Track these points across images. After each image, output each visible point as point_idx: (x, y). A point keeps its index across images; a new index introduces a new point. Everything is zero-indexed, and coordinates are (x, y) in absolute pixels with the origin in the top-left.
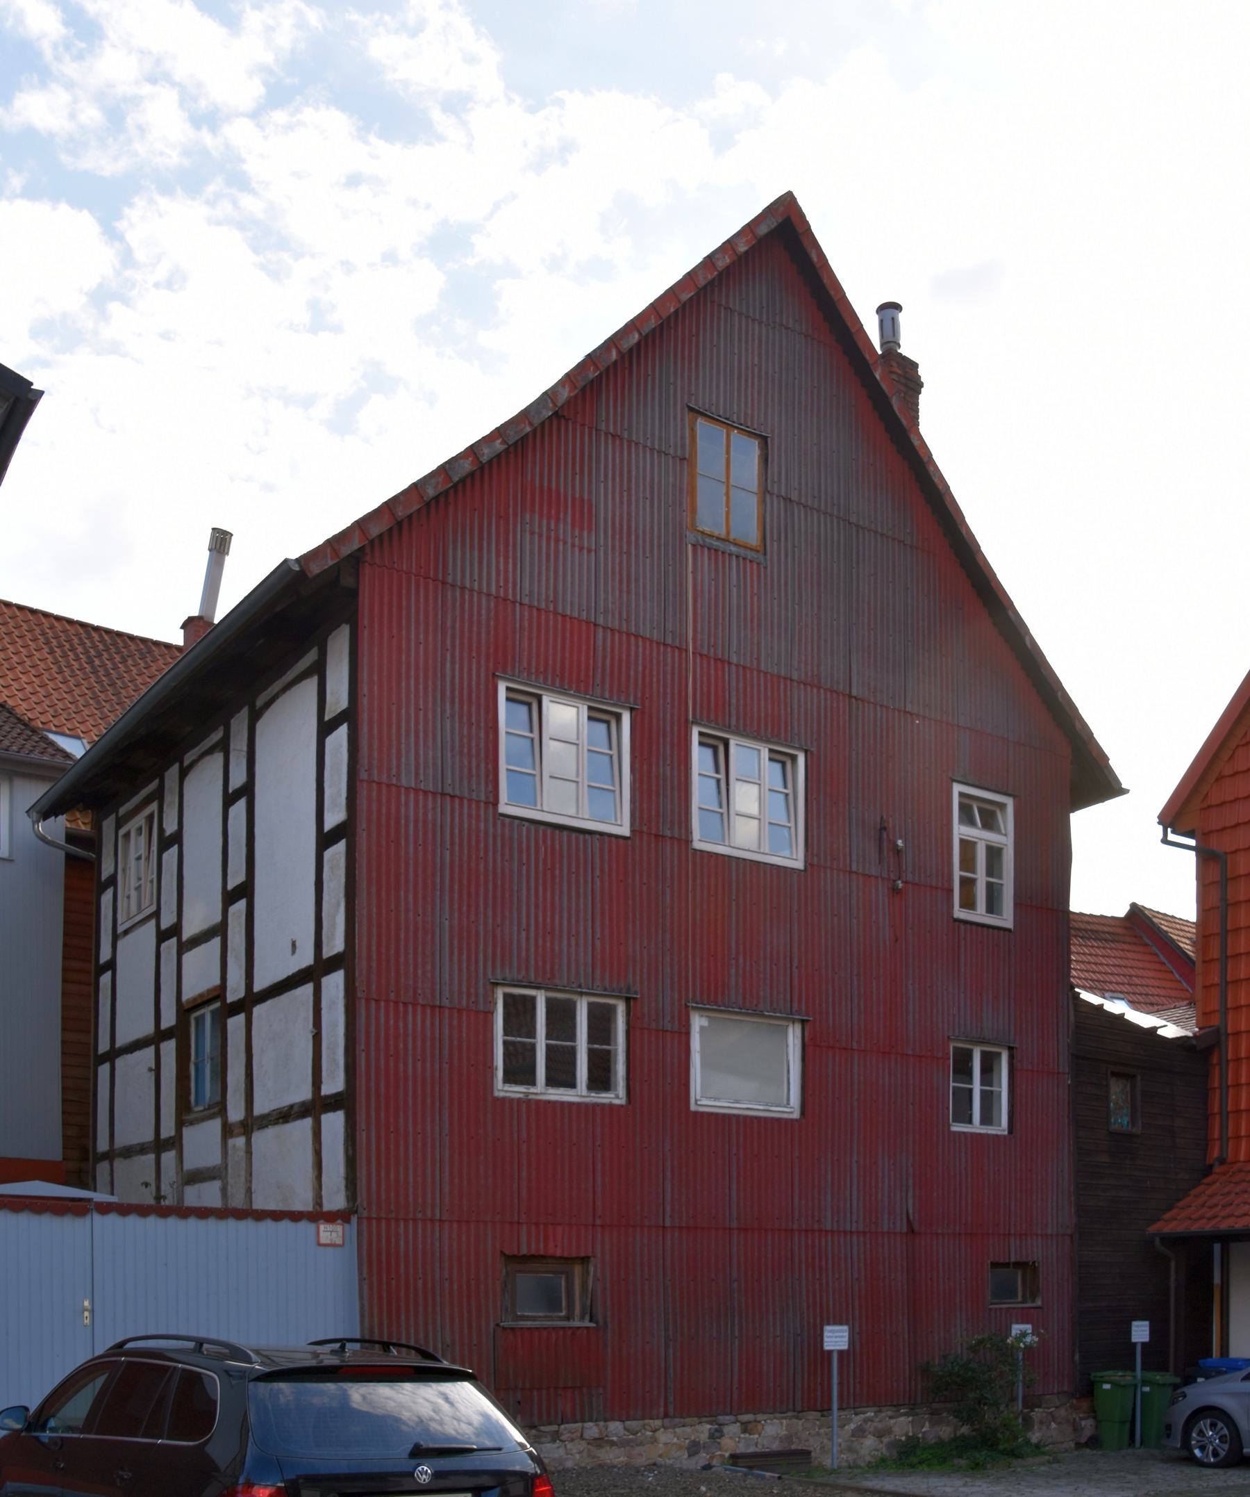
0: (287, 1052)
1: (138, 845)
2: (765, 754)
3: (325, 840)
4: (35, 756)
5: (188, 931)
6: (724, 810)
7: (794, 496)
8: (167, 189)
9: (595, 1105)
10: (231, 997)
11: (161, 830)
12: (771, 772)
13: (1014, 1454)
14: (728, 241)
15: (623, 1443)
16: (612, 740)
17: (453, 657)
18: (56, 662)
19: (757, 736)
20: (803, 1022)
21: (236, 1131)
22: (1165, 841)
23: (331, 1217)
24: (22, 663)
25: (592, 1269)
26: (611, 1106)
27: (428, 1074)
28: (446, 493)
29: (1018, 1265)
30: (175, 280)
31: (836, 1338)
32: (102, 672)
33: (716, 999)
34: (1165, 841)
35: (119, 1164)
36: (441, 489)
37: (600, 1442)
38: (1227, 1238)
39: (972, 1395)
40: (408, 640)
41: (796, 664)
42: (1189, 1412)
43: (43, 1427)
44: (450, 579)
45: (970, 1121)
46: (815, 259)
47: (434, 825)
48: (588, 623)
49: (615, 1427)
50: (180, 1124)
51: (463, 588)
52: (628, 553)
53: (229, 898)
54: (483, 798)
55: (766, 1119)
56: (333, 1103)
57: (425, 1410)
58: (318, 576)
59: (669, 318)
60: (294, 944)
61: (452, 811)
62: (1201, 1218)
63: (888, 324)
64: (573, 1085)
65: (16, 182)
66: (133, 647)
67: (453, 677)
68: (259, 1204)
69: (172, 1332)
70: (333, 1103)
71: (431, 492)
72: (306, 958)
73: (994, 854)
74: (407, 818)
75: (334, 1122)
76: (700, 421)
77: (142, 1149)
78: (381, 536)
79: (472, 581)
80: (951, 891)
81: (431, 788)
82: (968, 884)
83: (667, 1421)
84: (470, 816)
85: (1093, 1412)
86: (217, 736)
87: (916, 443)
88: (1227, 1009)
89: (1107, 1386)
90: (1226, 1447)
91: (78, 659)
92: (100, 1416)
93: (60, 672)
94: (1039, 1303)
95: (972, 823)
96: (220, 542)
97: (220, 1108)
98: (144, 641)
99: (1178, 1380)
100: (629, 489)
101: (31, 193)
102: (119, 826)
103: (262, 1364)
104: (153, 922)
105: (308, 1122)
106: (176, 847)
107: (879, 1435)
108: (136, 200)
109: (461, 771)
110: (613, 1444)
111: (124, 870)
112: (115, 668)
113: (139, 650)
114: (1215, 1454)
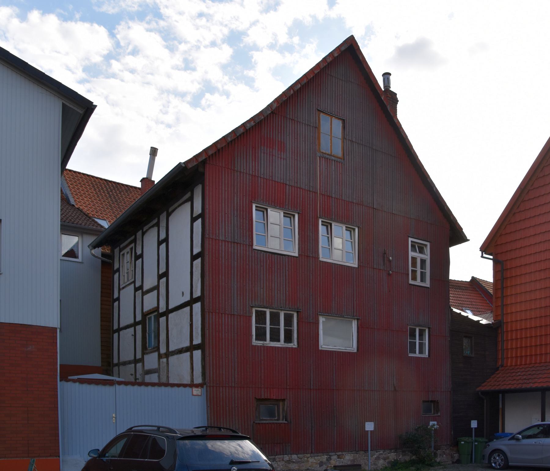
0: (181, 329)
1: (127, 257)
2: (344, 228)
3: (194, 258)
4: (91, 227)
5: (146, 288)
6: (330, 247)
7: (354, 140)
8: (132, 18)
9: (287, 348)
10: (161, 311)
11: (136, 253)
12: (346, 234)
13: (431, 465)
14: (331, 52)
16: (292, 224)
17: (237, 195)
18: (97, 193)
19: (342, 222)
20: (358, 319)
21: (163, 356)
22: (482, 257)
23: (197, 386)
24: (85, 194)
25: (286, 403)
26: (292, 348)
27: (230, 338)
28: (234, 140)
29: (432, 401)
30: (135, 52)
31: (370, 426)
32: (112, 197)
33: (328, 312)
34: (482, 257)
35: (121, 367)
36: (233, 138)
37: (289, 462)
38: (504, 392)
39: (416, 446)
40: (222, 189)
41: (355, 197)
42: (491, 451)
43: (104, 456)
44: (236, 169)
45: (415, 353)
46: (361, 58)
47: (231, 253)
48: (283, 184)
49: (294, 457)
50: (143, 354)
51: (240, 172)
52: (297, 160)
53: (160, 277)
54: (248, 244)
55: (345, 352)
56: (197, 347)
57: (233, 450)
58: (191, 168)
59: (311, 79)
60: (183, 293)
61: (237, 249)
62: (495, 385)
63: (386, 80)
64: (279, 341)
65: (78, 16)
66: (123, 188)
67: (237, 203)
68: (171, 381)
69: (150, 424)
70: (197, 347)
71: (229, 139)
72: (187, 298)
73: (423, 262)
74: (222, 251)
75: (197, 354)
76: (321, 114)
77: (130, 362)
78: (212, 155)
79: (244, 170)
80: (408, 274)
81: (230, 240)
82: (414, 272)
83: (312, 455)
84: (243, 250)
85: (458, 451)
86: (155, 221)
87: (396, 121)
88: (504, 314)
89: (463, 443)
90: (503, 463)
91: (104, 192)
92: (125, 452)
93: (98, 197)
94: (439, 414)
95: (416, 251)
96: (154, 152)
97: (158, 349)
98: (127, 186)
99: (487, 440)
100: (297, 139)
101: (83, 19)
102: (120, 251)
103: (180, 434)
104: (133, 285)
105: (188, 354)
106: (141, 259)
107: (385, 459)
108: (121, 22)
109: (240, 234)
110: (294, 462)
111: (122, 267)
112: (117, 195)
113: (125, 189)
114: (499, 465)
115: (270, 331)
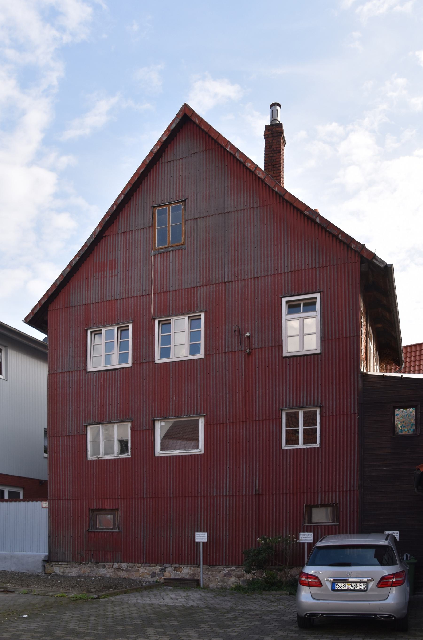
9: (121, 459)
15: (127, 571)
26: (126, 458)
49: (124, 565)
83: (143, 565)
107: (239, 577)
110: (123, 570)
115: (304, 433)
